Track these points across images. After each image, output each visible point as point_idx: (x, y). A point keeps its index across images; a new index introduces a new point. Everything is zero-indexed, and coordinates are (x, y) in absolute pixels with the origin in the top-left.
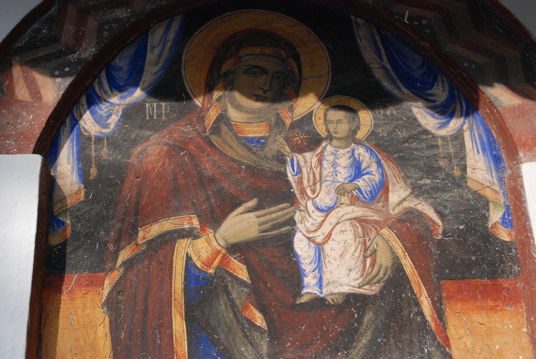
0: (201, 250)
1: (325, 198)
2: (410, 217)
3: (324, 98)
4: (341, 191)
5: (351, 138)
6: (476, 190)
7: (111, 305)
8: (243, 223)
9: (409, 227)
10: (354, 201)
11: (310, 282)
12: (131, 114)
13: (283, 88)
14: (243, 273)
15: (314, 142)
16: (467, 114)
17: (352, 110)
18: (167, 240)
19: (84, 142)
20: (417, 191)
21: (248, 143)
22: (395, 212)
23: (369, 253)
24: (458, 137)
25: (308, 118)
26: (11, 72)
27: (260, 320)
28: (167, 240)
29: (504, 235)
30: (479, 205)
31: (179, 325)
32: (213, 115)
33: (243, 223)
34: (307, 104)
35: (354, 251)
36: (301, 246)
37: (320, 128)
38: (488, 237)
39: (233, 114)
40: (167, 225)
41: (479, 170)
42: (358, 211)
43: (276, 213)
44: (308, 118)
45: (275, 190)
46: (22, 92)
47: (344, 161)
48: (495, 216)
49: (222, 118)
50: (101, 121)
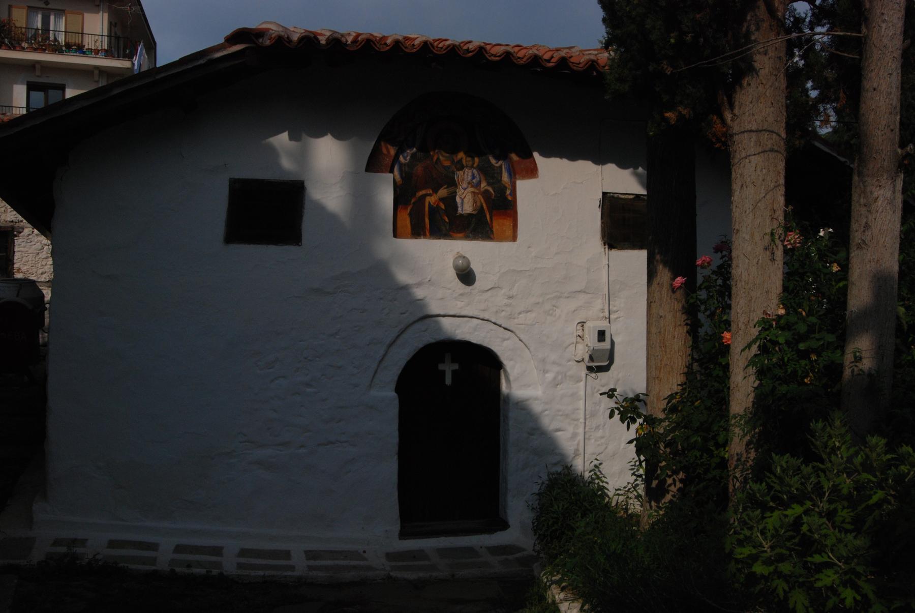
0: (432, 200)
1: (465, 185)
2: (487, 191)
3: (465, 153)
4: (469, 183)
5: (472, 167)
6: (434, 309)
7: (410, 214)
8: (443, 192)
9: (486, 194)
10: (472, 186)
11: (460, 209)
12: (413, 156)
13: (454, 151)
14: (443, 207)
15: (462, 168)
16: (504, 160)
17: (473, 158)
18: (424, 196)
19: (401, 165)
20: (489, 184)
21: (444, 167)
22: (482, 190)
23: (475, 202)
24: (501, 167)
25: (461, 160)
26: (508, 398)
27: (447, 220)
28: (424, 196)
29: (510, 198)
30: (504, 188)
31: (427, 221)
32: (435, 158)
33: (443, 192)
34: (461, 155)
35: (471, 201)
36: (458, 199)
37: (464, 163)
38: (506, 198)
39: (441, 157)
40: (423, 192)
41: (505, 177)
42: (473, 189)
43: (451, 189)
44: (461, 160)
45: (452, 183)
46: (385, 151)
47: (470, 174)
48: (508, 192)
49: (438, 159)
50: (405, 158)
